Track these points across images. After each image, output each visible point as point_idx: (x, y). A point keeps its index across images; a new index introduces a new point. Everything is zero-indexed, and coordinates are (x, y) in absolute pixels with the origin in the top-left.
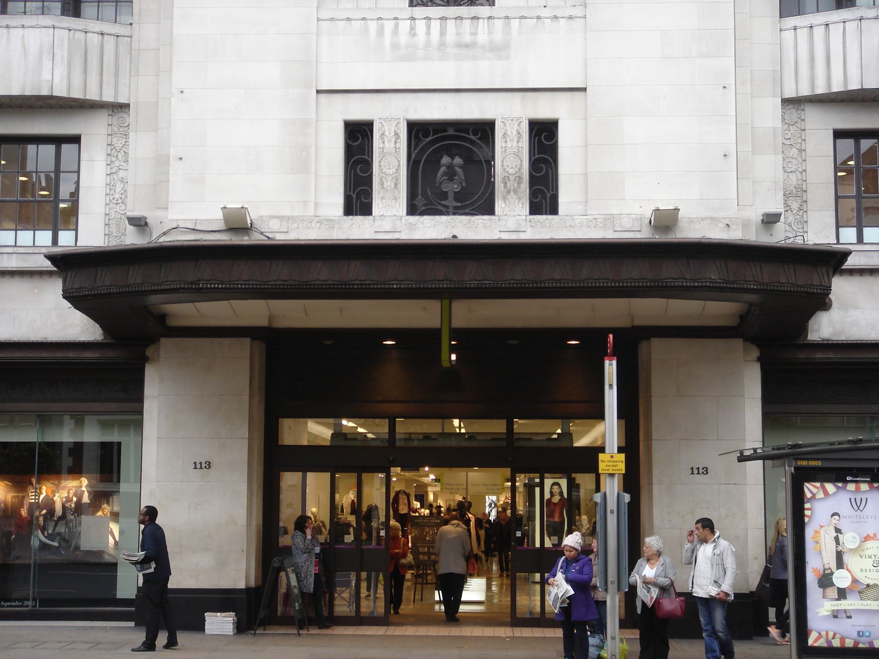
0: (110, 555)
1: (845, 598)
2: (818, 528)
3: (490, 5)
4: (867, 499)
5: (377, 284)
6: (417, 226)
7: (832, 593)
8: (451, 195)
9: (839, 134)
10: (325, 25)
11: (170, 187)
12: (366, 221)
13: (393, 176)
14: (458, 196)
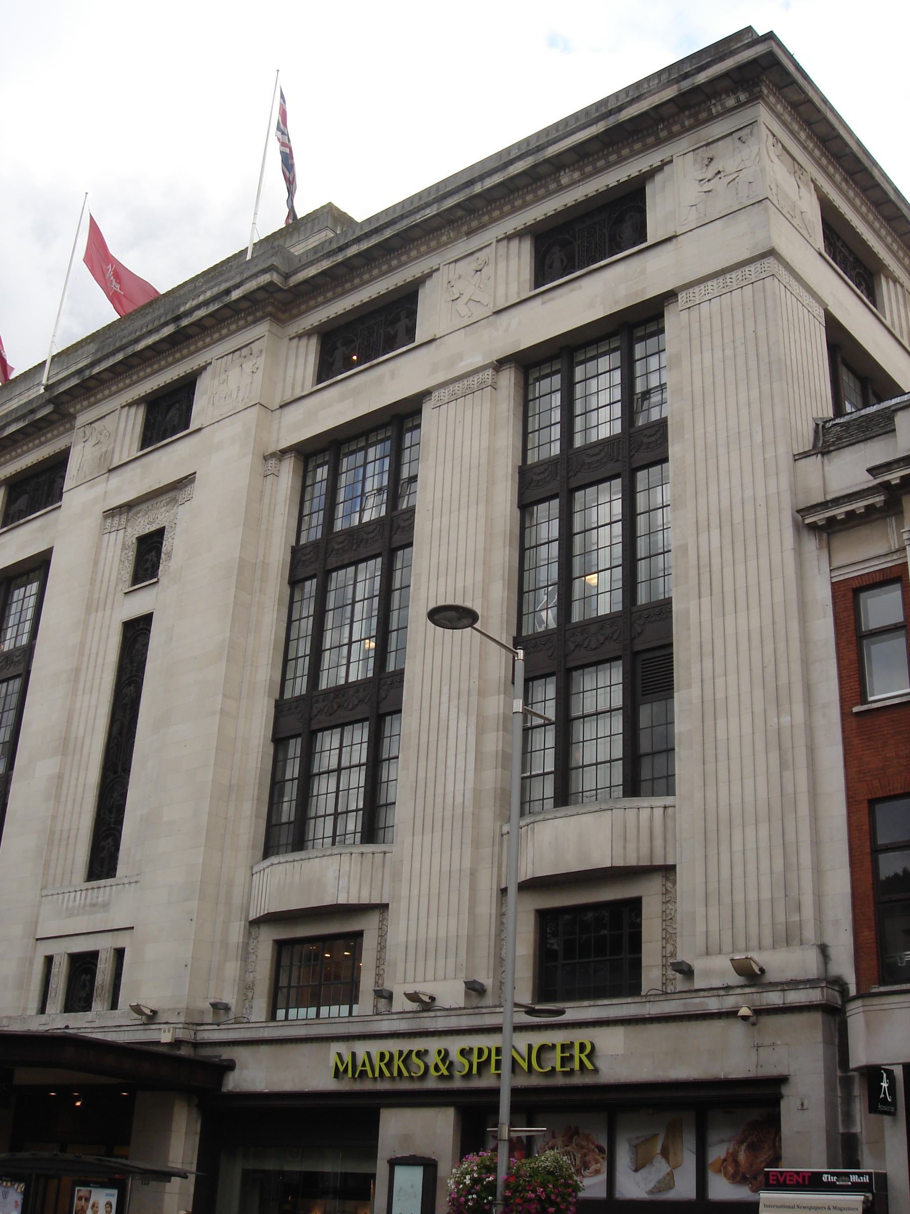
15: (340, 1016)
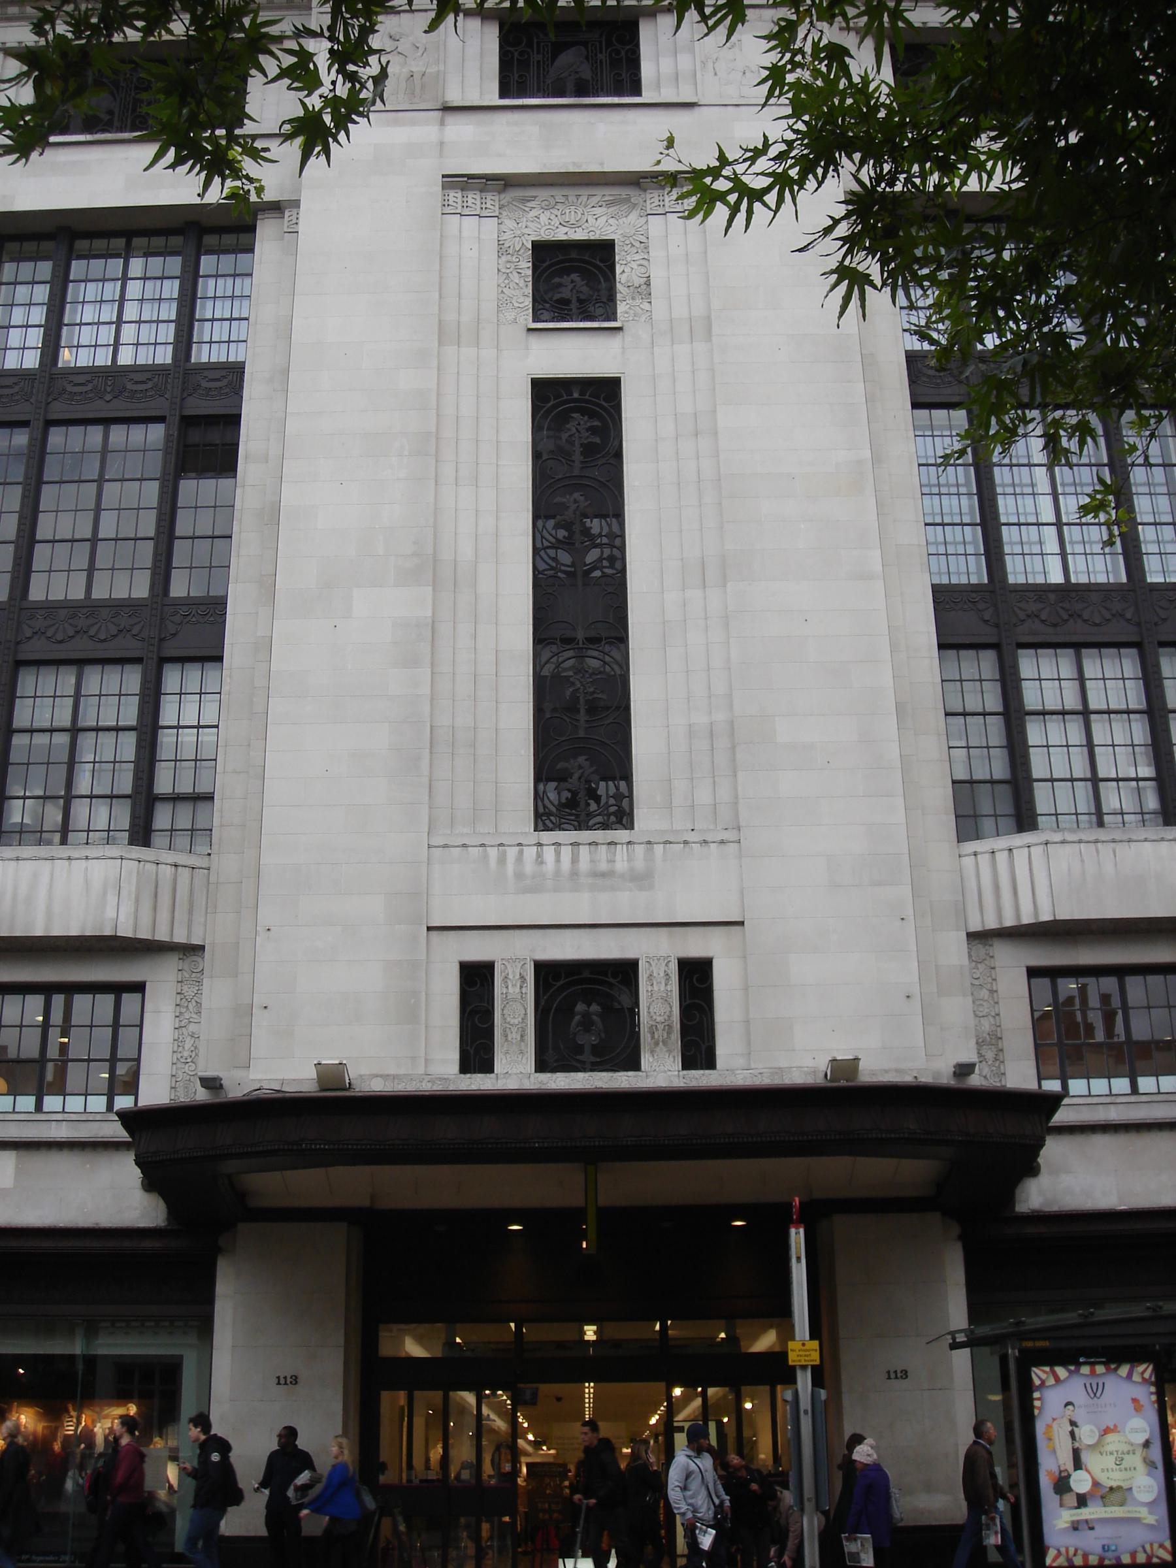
2: (1049, 1421)
4: (1104, 1384)
7: (1071, 1500)
8: (587, 1049)
9: (1033, 973)
10: (437, 852)
14: (596, 1050)
15: (16, 1110)
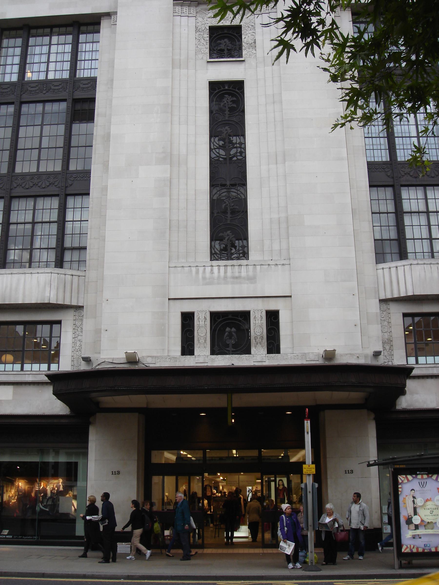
0: (72, 515)
1: (418, 529)
2: (405, 497)
3: (247, 260)
4: (426, 482)
5: (198, 387)
6: (215, 360)
7: (412, 527)
9: (405, 315)
11: (101, 344)
12: (192, 358)
13: (204, 337)
14: (234, 346)
15: (14, 370)
